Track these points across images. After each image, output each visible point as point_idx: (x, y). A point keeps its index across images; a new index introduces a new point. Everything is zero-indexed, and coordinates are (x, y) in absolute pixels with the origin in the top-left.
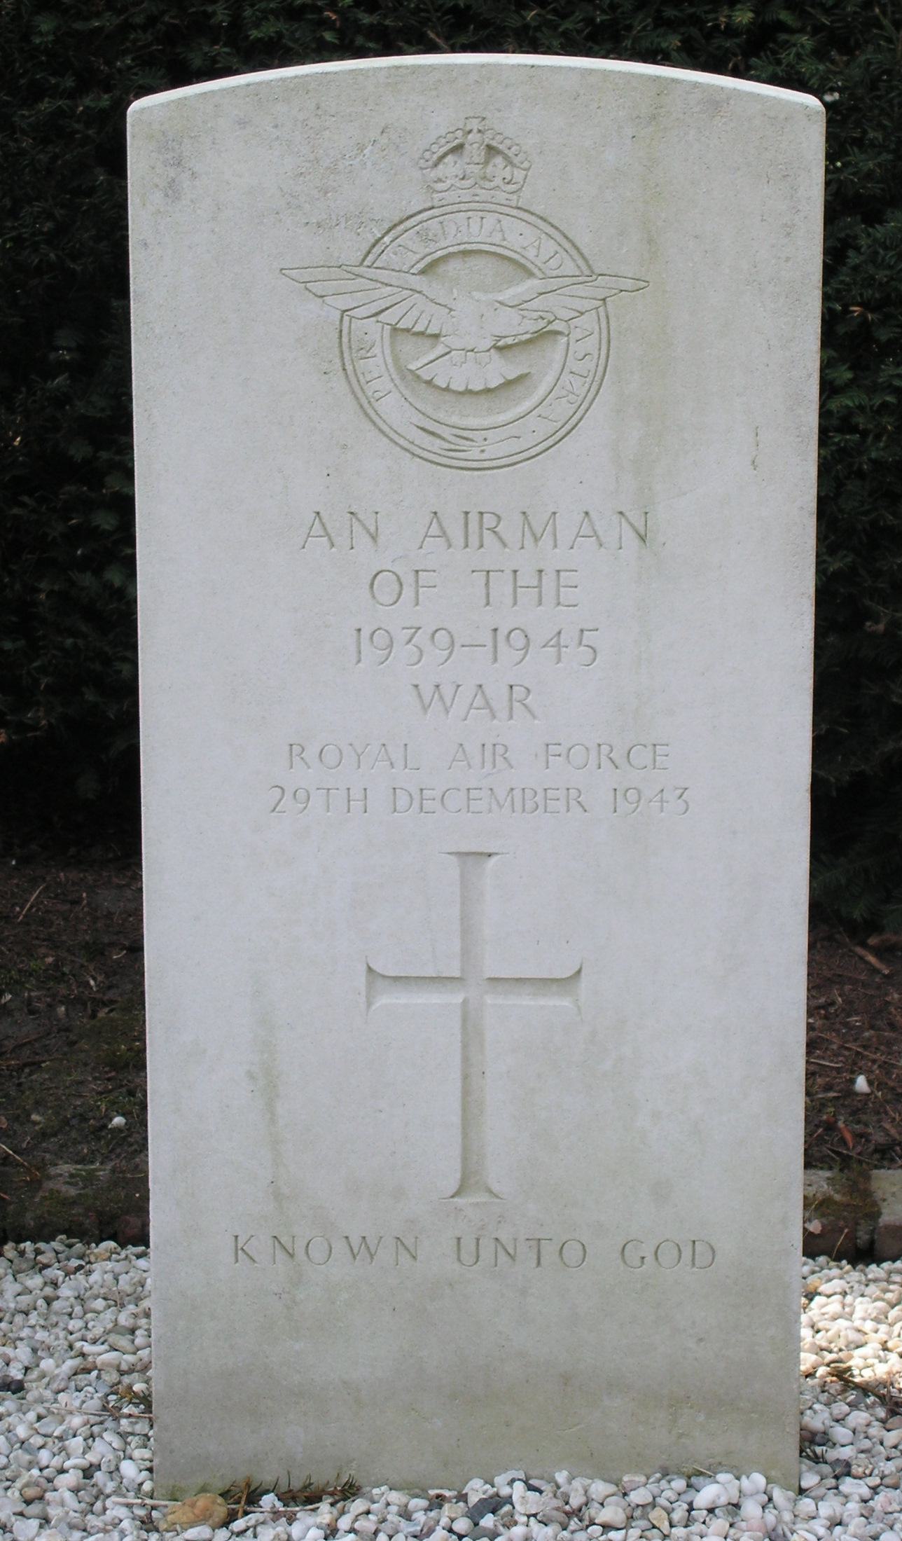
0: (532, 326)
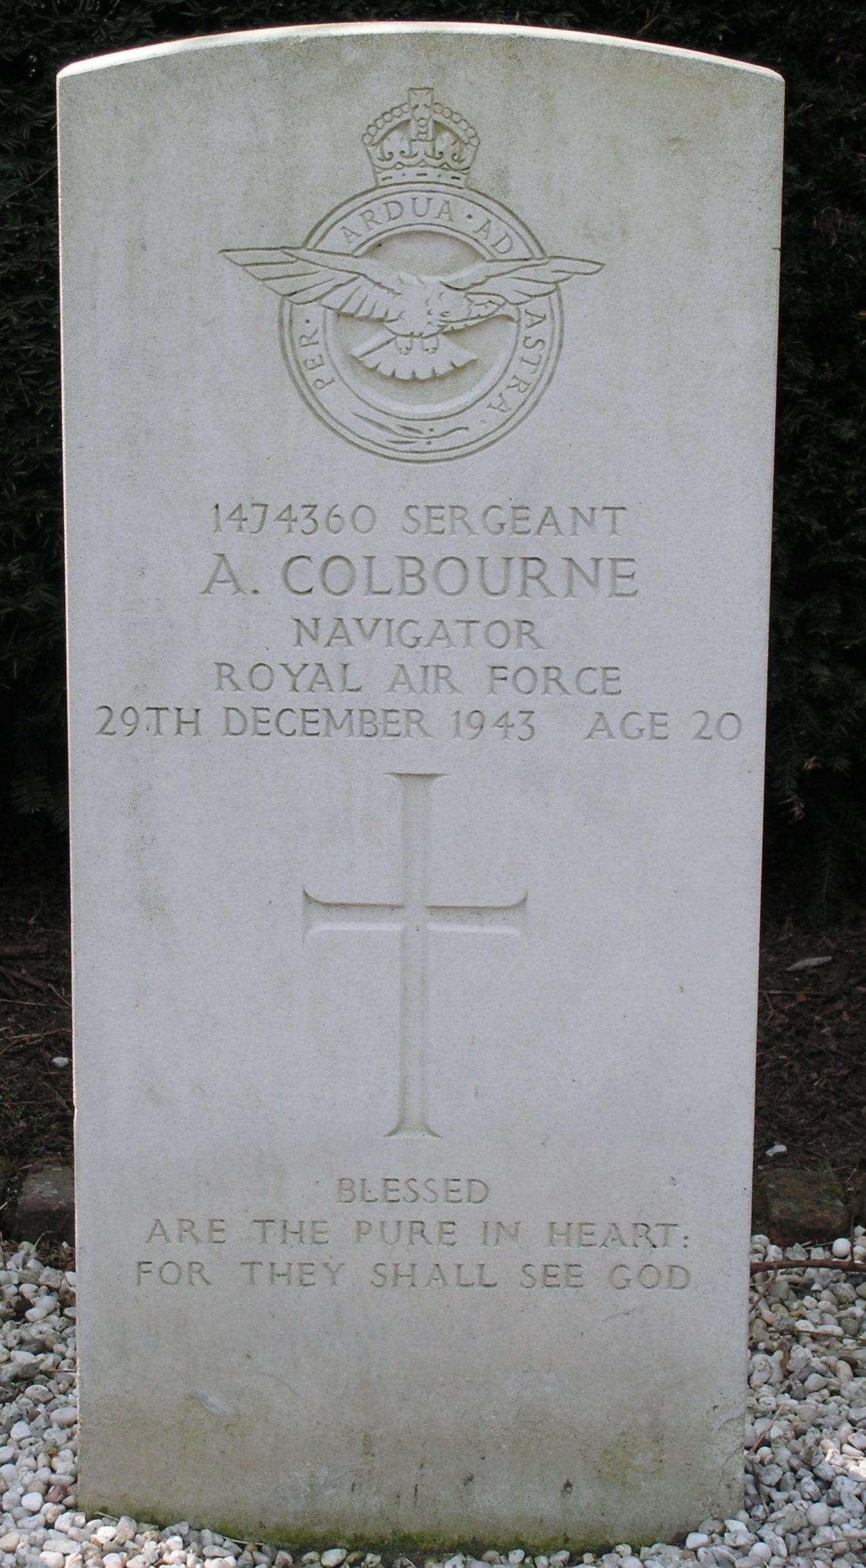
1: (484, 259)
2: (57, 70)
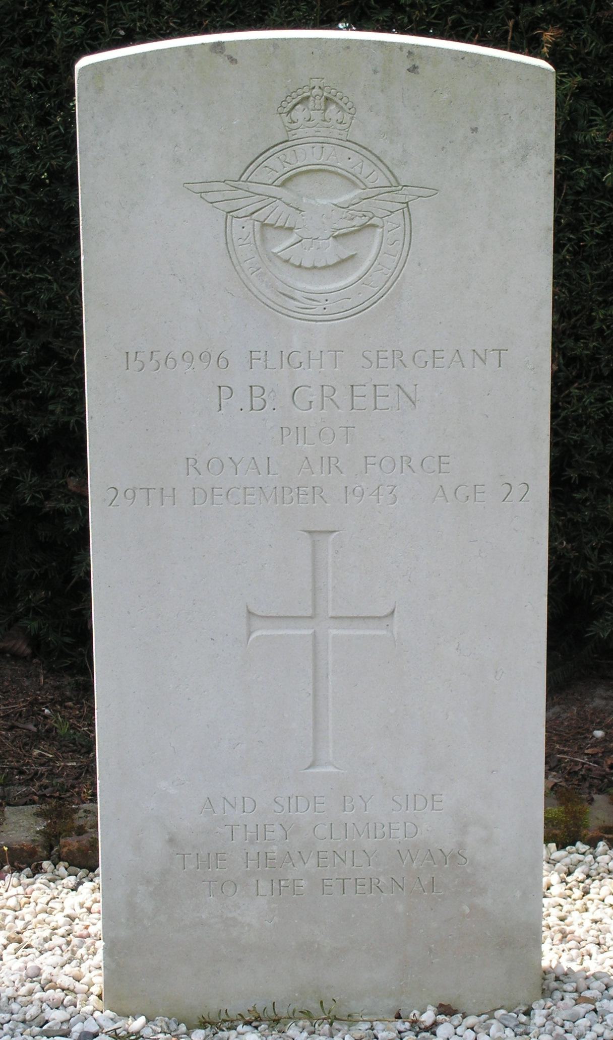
0: (358, 222)
2: (75, 61)
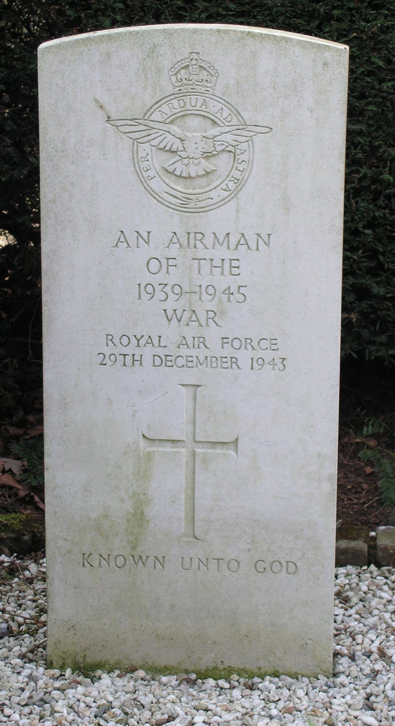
1: (219, 126)
